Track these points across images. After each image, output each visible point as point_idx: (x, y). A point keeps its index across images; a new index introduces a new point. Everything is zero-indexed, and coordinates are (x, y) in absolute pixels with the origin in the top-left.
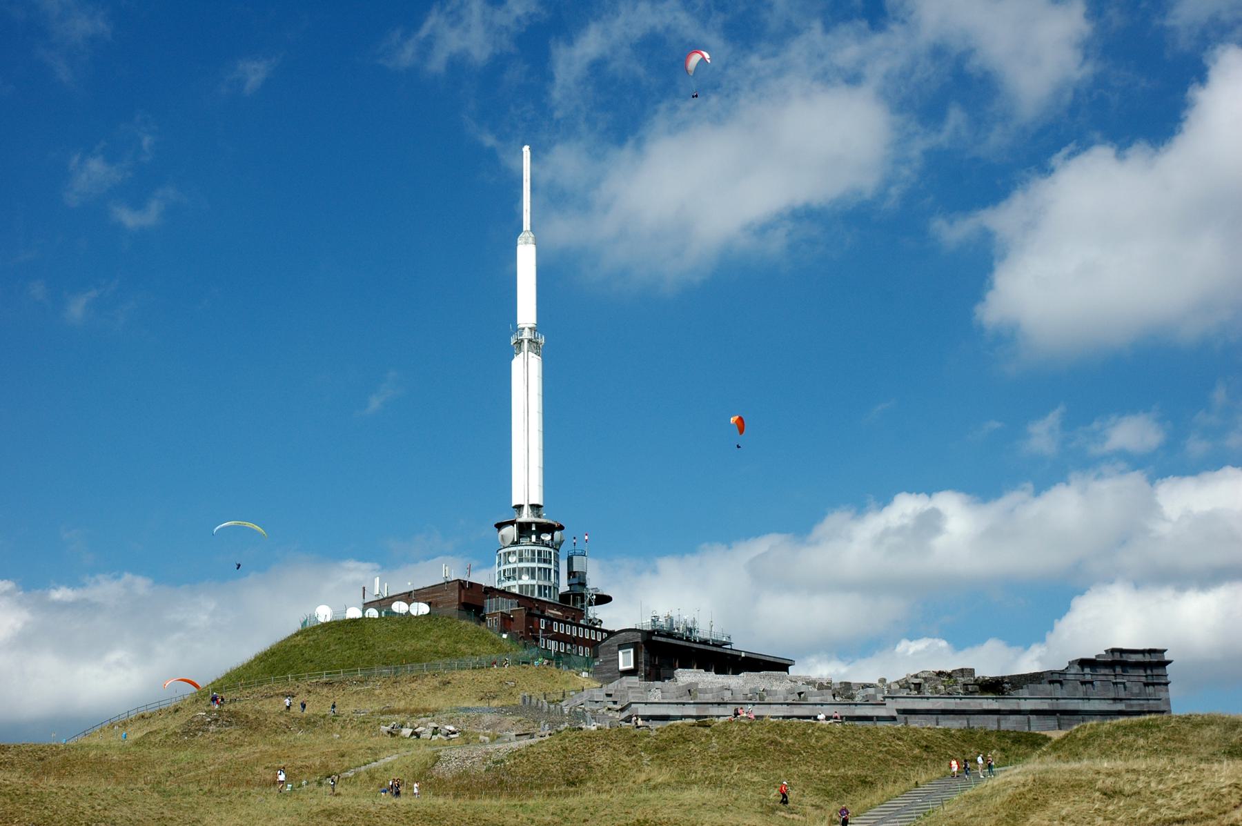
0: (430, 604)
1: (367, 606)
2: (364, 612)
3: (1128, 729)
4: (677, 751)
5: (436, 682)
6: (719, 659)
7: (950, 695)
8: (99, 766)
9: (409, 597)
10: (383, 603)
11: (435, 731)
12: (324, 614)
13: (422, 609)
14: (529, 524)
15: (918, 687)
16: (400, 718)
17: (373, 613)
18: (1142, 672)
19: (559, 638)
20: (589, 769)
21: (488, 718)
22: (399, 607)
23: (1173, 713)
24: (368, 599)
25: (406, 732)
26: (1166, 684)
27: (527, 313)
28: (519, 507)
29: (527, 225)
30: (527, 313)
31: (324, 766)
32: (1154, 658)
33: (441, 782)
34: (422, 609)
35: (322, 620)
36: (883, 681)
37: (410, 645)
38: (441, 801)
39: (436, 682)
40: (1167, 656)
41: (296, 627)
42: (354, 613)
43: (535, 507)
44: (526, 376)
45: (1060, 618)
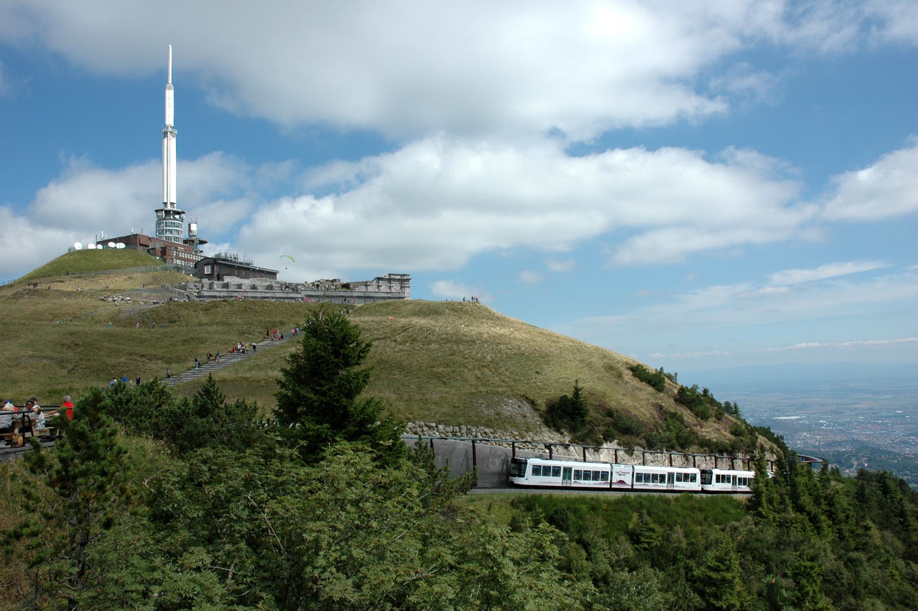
3: (381, 305)
4: (213, 310)
5: (126, 277)
6: (245, 270)
8: (35, 277)
9: (115, 241)
10: (104, 243)
11: (123, 299)
12: (78, 246)
13: (121, 246)
14: (170, 211)
15: (318, 286)
16: (108, 293)
18: (111, 287)
19: (182, 259)
20: (179, 317)
21: (145, 294)
25: (110, 299)
27: (170, 120)
28: (166, 204)
30: (170, 120)
31: (74, 313)
32: (406, 277)
33: (119, 321)
35: (77, 248)
37: (116, 261)
38: (118, 329)
39: (126, 277)
42: (92, 246)
43: (172, 204)
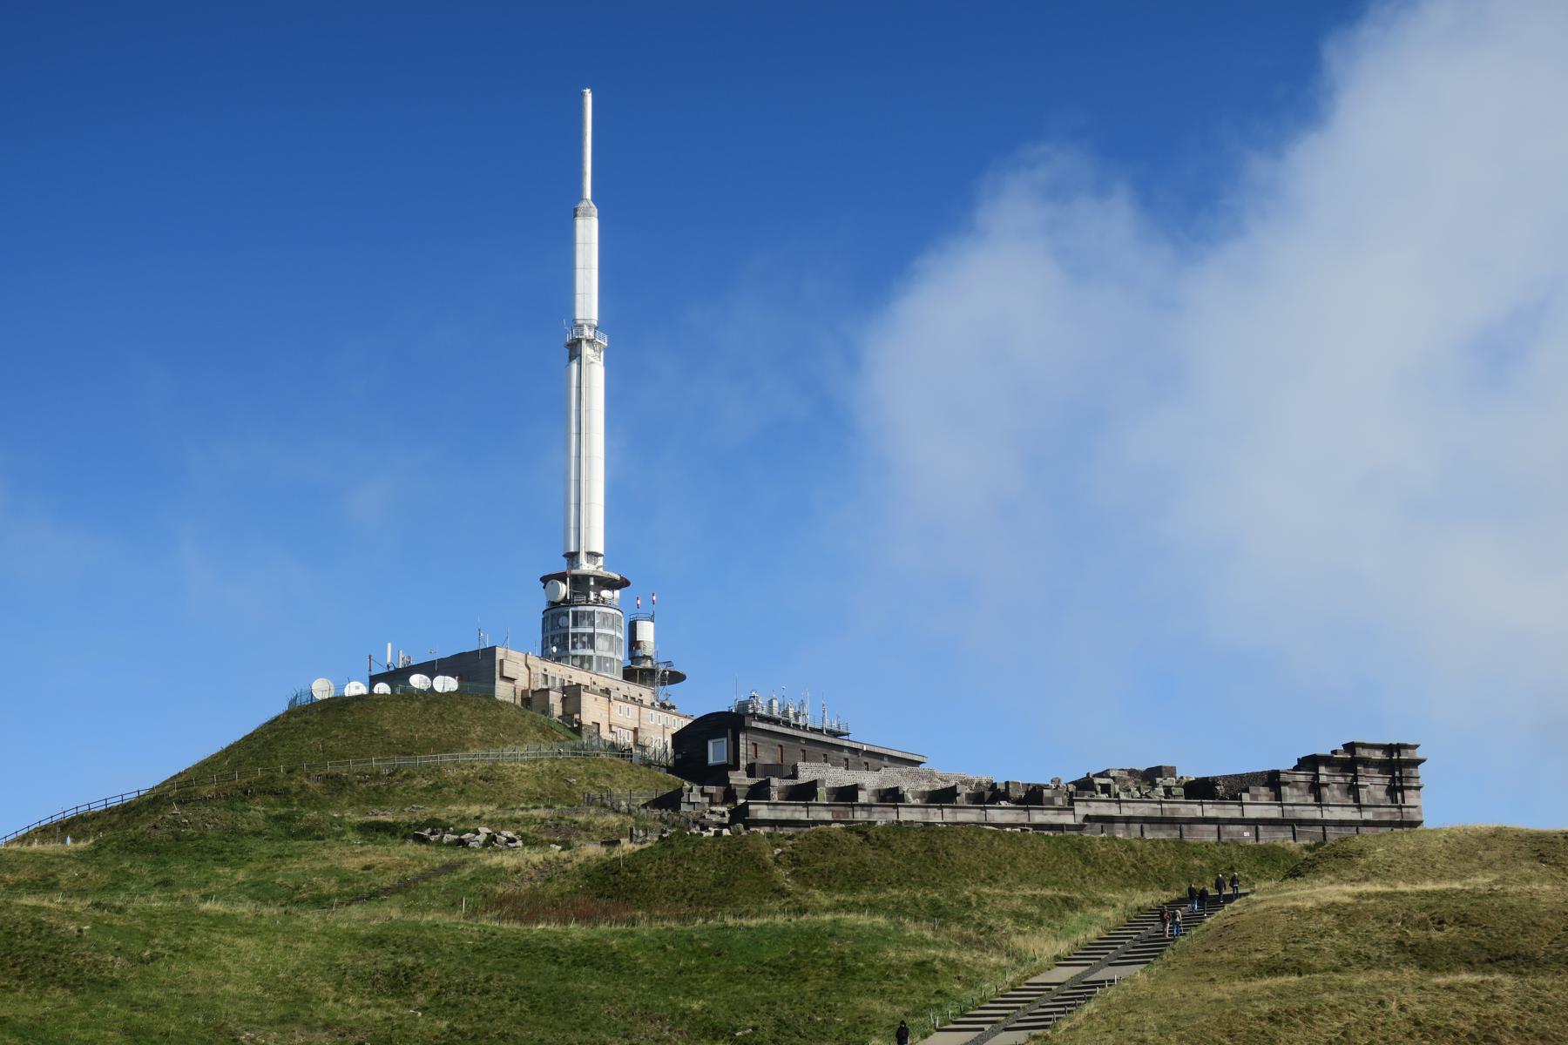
0: (462, 680)
1: (374, 680)
2: (371, 687)
7: (1145, 799)
9: (430, 669)
10: (397, 676)
12: (322, 689)
13: (446, 684)
17: (382, 688)
22: (417, 681)
23: (1428, 824)
24: (377, 671)
26: (1418, 788)
29: (588, 194)
34: (446, 684)
35: (319, 696)
36: (1057, 781)
40: (1418, 754)
41: (280, 708)
42: (356, 688)
44: (588, 230)
45: (730, 713)
